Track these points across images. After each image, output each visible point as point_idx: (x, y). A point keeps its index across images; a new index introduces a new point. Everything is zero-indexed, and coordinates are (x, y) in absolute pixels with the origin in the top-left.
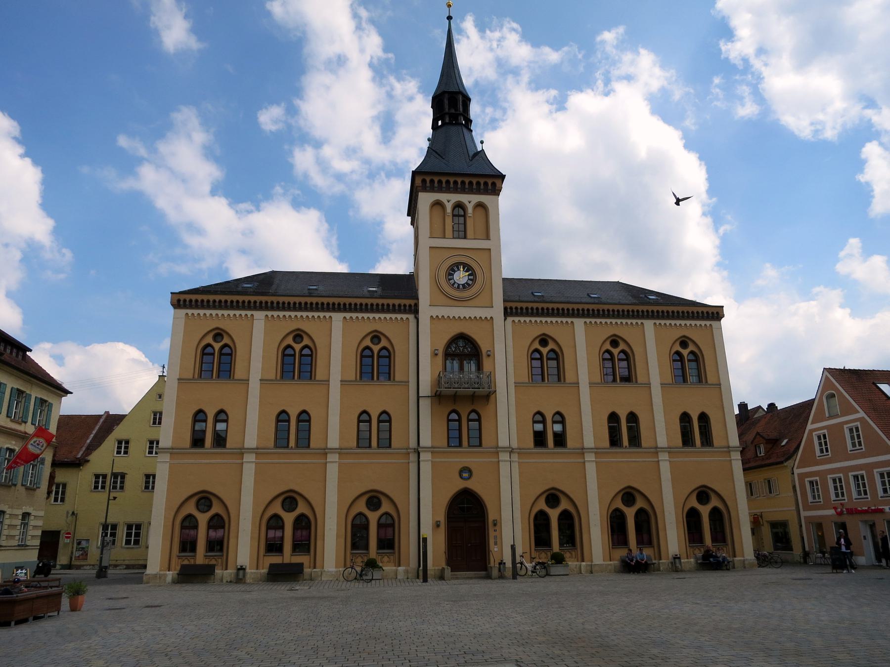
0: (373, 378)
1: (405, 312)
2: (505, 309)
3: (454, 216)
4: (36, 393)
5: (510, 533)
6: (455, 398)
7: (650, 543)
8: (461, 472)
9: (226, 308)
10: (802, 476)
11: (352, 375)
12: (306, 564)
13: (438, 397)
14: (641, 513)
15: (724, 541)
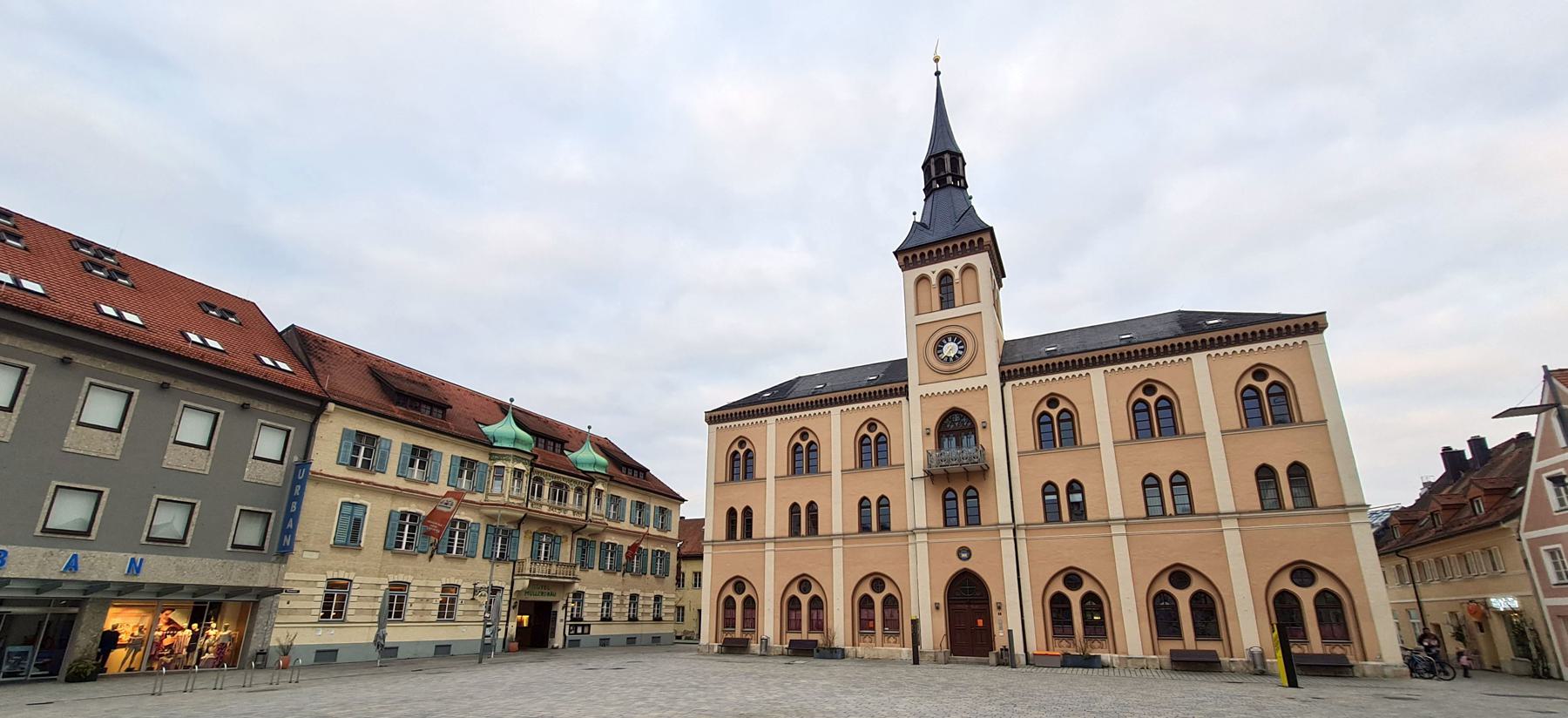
0: (1153, 435)
1: (897, 395)
2: (1002, 374)
3: (941, 286)
4: (653, 504)
5: (1018, 616)
6: (948, 476)
7: (1216, 636)
8: (959, 552)
9: (803, 409)
10: (1535, 544)
11: (1234, 421)
12: (1220, 652)
13: (931, 476)
14: (815, 599)
15: (1346, 636)
